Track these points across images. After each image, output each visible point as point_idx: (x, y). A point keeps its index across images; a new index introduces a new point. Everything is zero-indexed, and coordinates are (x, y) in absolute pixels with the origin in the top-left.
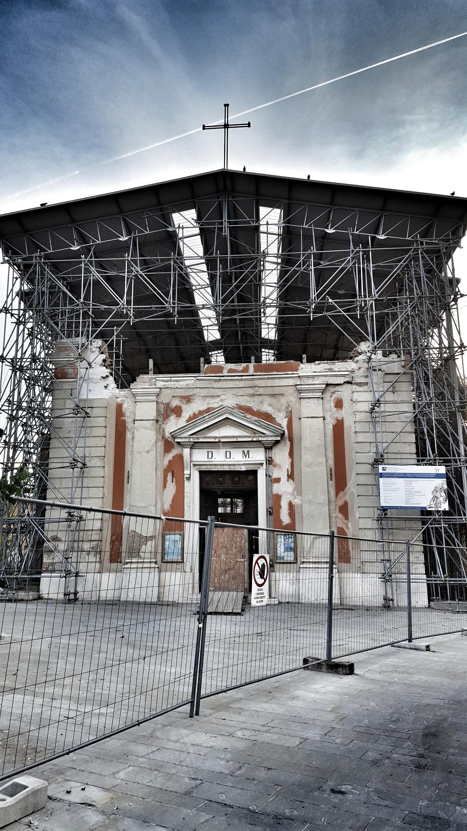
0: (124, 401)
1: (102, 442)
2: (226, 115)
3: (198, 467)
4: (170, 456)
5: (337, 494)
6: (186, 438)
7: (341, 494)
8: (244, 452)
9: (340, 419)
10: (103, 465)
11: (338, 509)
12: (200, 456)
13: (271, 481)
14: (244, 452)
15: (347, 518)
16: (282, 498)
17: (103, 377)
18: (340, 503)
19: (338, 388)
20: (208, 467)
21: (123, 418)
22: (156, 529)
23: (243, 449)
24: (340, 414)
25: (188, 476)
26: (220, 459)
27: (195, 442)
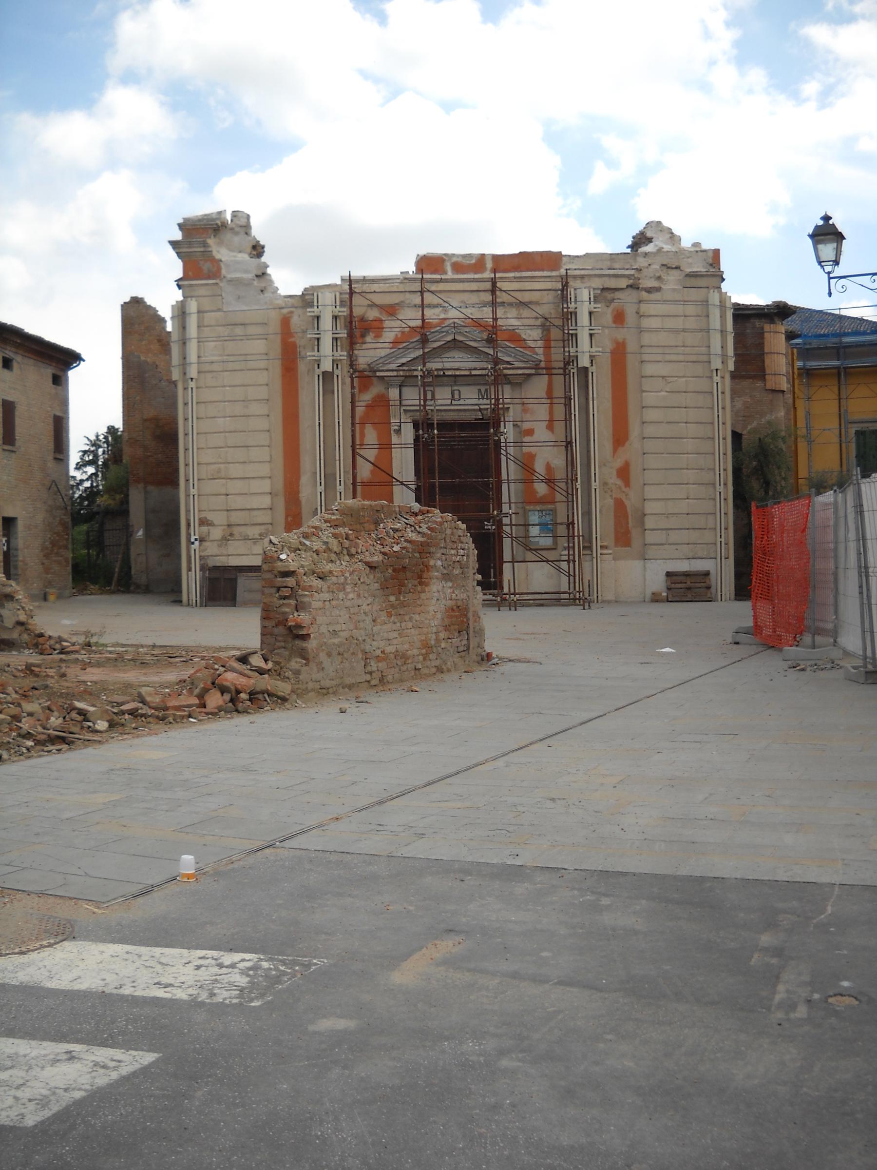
0: (292, 312)
1: (649, 430)
2: (516, 525)
3: (412, 414)
4: (367, 397)
5: (615, 450)
6: (392, 371)
7: (621, 450)
8: (480, 390)
9: (621, 341)
10: (267, 413)
11: (615, 473)
12: (412, 397)
13: (520, 433)
14: (480, 390)
15: (627, 484)
16: (537, 458)
17: (257, 276)
18: (619, 463)
19: (618, 295)
20: (461, 413)
21: (292, 340)
22: (118, 661)
23: (479, 387)
24: (621, 334)
25: (396, 428)
26: (443, 401)
27: (406, 377)
